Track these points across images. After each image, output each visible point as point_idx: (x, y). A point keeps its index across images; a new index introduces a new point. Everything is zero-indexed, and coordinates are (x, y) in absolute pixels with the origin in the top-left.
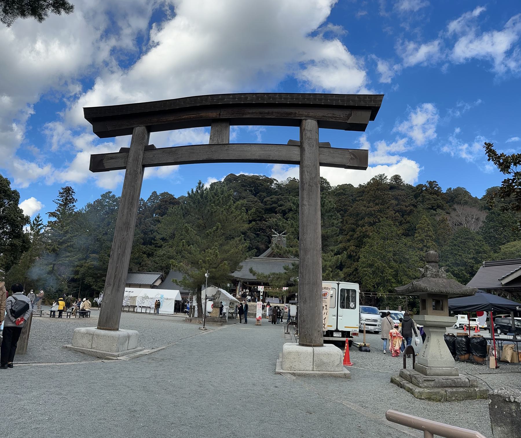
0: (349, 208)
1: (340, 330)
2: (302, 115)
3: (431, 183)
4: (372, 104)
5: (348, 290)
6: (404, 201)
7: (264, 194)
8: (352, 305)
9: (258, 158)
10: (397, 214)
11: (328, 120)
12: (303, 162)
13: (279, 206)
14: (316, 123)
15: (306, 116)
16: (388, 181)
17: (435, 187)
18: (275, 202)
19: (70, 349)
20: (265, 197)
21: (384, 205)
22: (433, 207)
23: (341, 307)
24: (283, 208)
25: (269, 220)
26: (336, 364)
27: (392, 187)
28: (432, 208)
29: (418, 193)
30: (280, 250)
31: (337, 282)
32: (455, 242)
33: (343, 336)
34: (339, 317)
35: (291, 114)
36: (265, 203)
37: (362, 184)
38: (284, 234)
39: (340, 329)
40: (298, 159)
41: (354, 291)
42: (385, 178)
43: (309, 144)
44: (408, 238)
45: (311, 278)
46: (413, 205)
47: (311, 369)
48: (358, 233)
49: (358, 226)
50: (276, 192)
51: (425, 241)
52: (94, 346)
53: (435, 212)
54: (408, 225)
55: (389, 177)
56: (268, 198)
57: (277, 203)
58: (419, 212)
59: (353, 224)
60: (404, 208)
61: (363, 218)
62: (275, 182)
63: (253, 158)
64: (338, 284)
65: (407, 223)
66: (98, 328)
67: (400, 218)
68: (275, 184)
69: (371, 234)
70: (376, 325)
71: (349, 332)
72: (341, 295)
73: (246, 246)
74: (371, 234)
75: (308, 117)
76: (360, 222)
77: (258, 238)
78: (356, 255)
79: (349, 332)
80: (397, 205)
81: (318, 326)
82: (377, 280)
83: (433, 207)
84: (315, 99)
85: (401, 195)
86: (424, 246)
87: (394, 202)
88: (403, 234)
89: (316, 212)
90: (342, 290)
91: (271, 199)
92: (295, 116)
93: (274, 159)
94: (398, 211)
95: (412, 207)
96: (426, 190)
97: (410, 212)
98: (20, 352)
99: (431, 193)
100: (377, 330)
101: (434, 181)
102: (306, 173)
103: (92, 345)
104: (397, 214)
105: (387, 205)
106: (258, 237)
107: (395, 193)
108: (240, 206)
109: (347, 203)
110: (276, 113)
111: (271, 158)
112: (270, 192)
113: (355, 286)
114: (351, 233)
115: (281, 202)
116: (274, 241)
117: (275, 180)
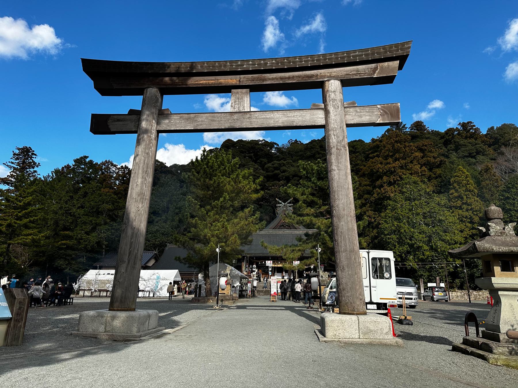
0: (362, 167)
1: (375, 302)
2: (324, 77)
3: (464, 125)
4: (400, 53)
5: (381, 259)
6: (431, 152)
7: (265, 160)
8: (387, 275)
9: (281, 125)
10: (424, 167)
11: (352, 78)
12: (328, 126)
13: (282, 172)
14: (340, 83)
15: (328, 77)
16: (407, 130)
17: (471, 129)
18: (276, 168)
19: (76, 336)
20: (265, 164)
21: (405, 159)
22: (470, 154)
23: (374, 277)
24: (286, 174)
25: (272, 189)
26: (385, 332)
27: (414, 137)
28: (470, 156)
29: (448, 138)
30: (293, 220)
31: (367, 251)
32: (507, 195)
33: (378, 309)
34: (372, 288)
35: (312, 76)
36: (267, 170)
37: (375, 138)
38: (289, 203)
39: (374, 301)
40: (323, 122)
41: (389, 259)
42: (403, 127)
43: (334, 106)
44: (441, 195)
45: (348, 245)
46: (443, 155)
47: (357, 337)
48: (375, 195)
49: (375, 187)
50: (278, 157)
51: (465, 197)
52: (108, 329)
53: (473, 160)
54: (439, 180)
55: (408, 126)
56: (270, 165)
57: (279, 169)
58: (452, 163)
59: (369, 185)
60: (432, 160)
61: (381, 177)
62: (275, 146)
63: (277, 125)
64: (368, 253)
65: (436, 178)
66: (109, 310)
67: (428, 173)
68: (276, 148)
69: (392, 195)
70: (411, 299)
71: (385, 304)
72: (372, 264)
73: (257, 218)
74: (392, 195)
75: (331, 78)
76: (378, 183)
77: (261, 209)
78: (375, 221)
79: (386, 304)
80: (422, 158)
81: (360, 294)
82: (406, 248)
83: (470, 154)
84: (337, 58)
85: (426, 146)
86: (463, 204)
87: (418, 154)
88: (434, 192)
89: (347, 177)
90: (373, 259)
91: (273, 164)
92: (317, 79)
93: (298, 125)
94: (424, 164)
95: (442, 158)
96: (458, 134)
97: (440, 164)
98: (14, 343)
99: (466, 138)
100: (413, 304)
101: (468, 123)
102: (333, 136)
103: (105, 328)
104: (424, 167)
105: (408, 160)
106: (261, 207)
107: (420, 143)
108: (247, 175)
109: (359, 162)
110: (297, 77)
111: (295, 124)
112: (270, 157)
113: (389, 254)
114: (366, 196)
115: (284, 168)
116: (279, 211)
117: (276, 144)
